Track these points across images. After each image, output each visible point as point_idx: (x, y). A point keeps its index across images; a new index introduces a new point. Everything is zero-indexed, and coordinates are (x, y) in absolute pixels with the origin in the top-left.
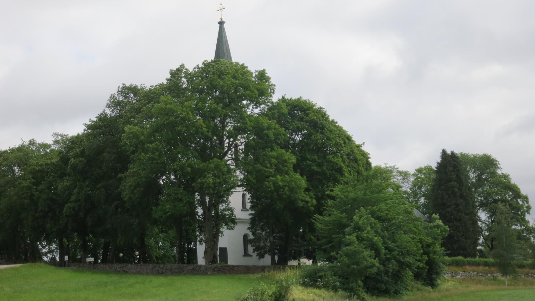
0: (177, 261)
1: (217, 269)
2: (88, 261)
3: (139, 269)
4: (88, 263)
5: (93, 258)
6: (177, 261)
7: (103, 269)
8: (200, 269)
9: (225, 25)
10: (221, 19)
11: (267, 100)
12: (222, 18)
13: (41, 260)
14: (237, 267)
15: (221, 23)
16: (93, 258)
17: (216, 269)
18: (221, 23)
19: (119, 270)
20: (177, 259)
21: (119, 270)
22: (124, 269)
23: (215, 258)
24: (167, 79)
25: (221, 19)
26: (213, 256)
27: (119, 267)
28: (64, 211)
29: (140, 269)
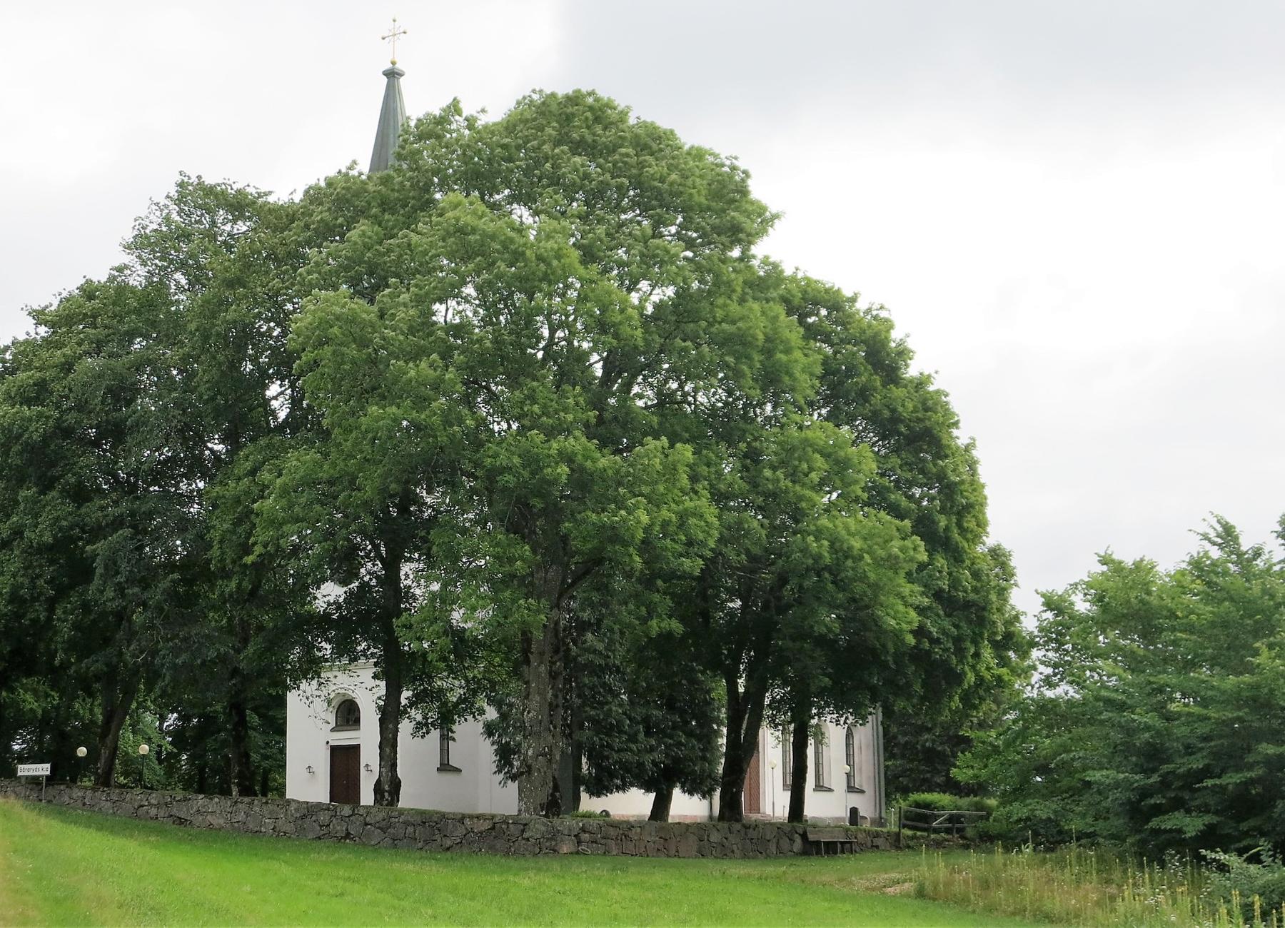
0: (386, 795)
1: (587, 835)
2: (26, 773)
3: (241, 817)
4: (23, 781)
5: (48, 766)
6: (386, 795)
7: (84, 804)
8: (523, 831)
9: (402, 80)
10: (393, 63)
11: (477, 265)
12: (396, 60)
13: (12, 774)
14: (639, 830)
15: (392, 75)
16: (48, 766)
17: (585, 836)
18: (392, 75)
19: (153, 812)
20: (386, 788)
21: (153, 812)
22: (175, 812)
23: (557, 794)
24: (128, 247)
25: (393, 63)
26: (551, 785)
27: (153, 801)
28: (1161, 676)
29: (247, 815)
